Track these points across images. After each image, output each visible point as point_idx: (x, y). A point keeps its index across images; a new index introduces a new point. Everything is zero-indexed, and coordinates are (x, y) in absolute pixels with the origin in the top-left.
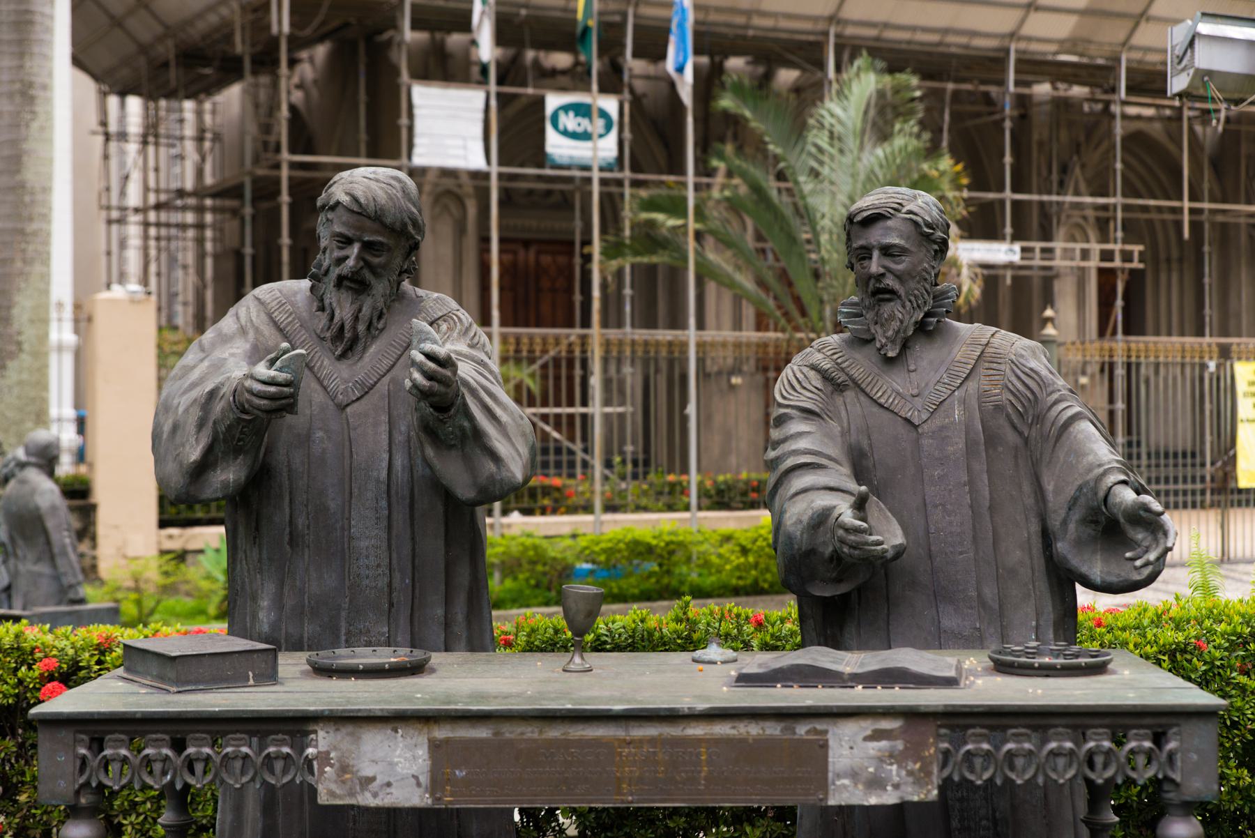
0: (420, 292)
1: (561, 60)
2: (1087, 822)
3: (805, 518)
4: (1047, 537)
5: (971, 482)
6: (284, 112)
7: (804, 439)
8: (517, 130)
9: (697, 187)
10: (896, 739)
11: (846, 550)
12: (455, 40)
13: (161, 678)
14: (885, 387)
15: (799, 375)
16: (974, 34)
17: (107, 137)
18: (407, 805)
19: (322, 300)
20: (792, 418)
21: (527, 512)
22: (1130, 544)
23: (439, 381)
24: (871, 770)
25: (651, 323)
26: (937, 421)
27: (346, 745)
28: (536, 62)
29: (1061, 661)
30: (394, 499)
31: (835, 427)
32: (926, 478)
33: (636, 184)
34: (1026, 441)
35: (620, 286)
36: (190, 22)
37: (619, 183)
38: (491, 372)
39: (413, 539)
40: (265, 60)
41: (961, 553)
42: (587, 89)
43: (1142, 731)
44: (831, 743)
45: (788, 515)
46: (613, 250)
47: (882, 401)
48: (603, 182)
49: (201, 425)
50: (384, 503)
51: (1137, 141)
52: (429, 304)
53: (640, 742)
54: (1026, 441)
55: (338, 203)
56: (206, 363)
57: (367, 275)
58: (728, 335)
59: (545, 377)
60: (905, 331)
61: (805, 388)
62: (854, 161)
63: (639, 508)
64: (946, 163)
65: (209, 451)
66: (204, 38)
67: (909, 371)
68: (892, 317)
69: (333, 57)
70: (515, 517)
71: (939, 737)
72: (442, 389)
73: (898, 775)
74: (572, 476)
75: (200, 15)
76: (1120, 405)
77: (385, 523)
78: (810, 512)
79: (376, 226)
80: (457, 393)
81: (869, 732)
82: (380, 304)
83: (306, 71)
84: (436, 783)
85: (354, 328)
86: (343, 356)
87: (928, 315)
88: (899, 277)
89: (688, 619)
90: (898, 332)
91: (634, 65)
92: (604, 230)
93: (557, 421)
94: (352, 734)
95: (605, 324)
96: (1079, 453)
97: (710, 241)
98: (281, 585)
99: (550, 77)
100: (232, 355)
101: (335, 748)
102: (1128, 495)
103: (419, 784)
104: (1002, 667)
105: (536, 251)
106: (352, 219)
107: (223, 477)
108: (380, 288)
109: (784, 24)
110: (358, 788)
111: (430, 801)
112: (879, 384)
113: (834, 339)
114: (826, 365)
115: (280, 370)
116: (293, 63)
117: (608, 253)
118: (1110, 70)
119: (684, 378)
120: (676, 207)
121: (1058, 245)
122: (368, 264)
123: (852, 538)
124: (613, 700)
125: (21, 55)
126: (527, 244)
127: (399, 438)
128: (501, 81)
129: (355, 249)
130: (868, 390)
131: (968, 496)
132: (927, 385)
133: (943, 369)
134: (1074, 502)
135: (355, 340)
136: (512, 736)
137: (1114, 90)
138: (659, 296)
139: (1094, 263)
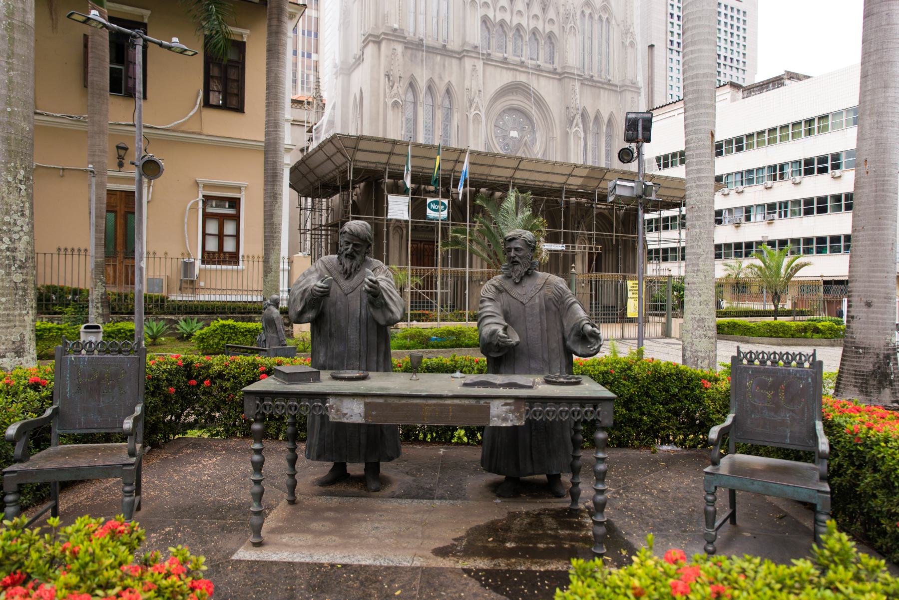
2: (574, 429)
6: (351, 202)
8: (418, 209)
13: (284, 379)
21: (418, 321)
22: (590, 343)
25: (457, 266)
26: (531, 303)
27: (338, 403)
29: (565, 381)
31: (499, 304)
33: (452, 225)
40: (346, 187)
49: (301, 300)
51: (600, 215)
58: (479, 270)
59: (424, 280)
62: (515, 222)
64: (541, 219)
65: (304, 308)
69: (365, 186)
70: (415, 322)
76: (594, 293)
80: (380, 291)
86: (347, 279)
88: (520, 257)
93: (427, 294)
96: (575, 314)
102: (589, 328)
104: (548, 382)
105: (422, 244)
108: (359, 258)
114: (497, 284)
116: (354, 188)
118: (593, 194)
120: (463, 232)
121: (577, 245)
124: (422, 391)
126: (421, 242)
127: (363, 305)
129: (351, 246)
134: (572, 329)
135: (351, 274)
138: (458, 258)
139: (587, 251)
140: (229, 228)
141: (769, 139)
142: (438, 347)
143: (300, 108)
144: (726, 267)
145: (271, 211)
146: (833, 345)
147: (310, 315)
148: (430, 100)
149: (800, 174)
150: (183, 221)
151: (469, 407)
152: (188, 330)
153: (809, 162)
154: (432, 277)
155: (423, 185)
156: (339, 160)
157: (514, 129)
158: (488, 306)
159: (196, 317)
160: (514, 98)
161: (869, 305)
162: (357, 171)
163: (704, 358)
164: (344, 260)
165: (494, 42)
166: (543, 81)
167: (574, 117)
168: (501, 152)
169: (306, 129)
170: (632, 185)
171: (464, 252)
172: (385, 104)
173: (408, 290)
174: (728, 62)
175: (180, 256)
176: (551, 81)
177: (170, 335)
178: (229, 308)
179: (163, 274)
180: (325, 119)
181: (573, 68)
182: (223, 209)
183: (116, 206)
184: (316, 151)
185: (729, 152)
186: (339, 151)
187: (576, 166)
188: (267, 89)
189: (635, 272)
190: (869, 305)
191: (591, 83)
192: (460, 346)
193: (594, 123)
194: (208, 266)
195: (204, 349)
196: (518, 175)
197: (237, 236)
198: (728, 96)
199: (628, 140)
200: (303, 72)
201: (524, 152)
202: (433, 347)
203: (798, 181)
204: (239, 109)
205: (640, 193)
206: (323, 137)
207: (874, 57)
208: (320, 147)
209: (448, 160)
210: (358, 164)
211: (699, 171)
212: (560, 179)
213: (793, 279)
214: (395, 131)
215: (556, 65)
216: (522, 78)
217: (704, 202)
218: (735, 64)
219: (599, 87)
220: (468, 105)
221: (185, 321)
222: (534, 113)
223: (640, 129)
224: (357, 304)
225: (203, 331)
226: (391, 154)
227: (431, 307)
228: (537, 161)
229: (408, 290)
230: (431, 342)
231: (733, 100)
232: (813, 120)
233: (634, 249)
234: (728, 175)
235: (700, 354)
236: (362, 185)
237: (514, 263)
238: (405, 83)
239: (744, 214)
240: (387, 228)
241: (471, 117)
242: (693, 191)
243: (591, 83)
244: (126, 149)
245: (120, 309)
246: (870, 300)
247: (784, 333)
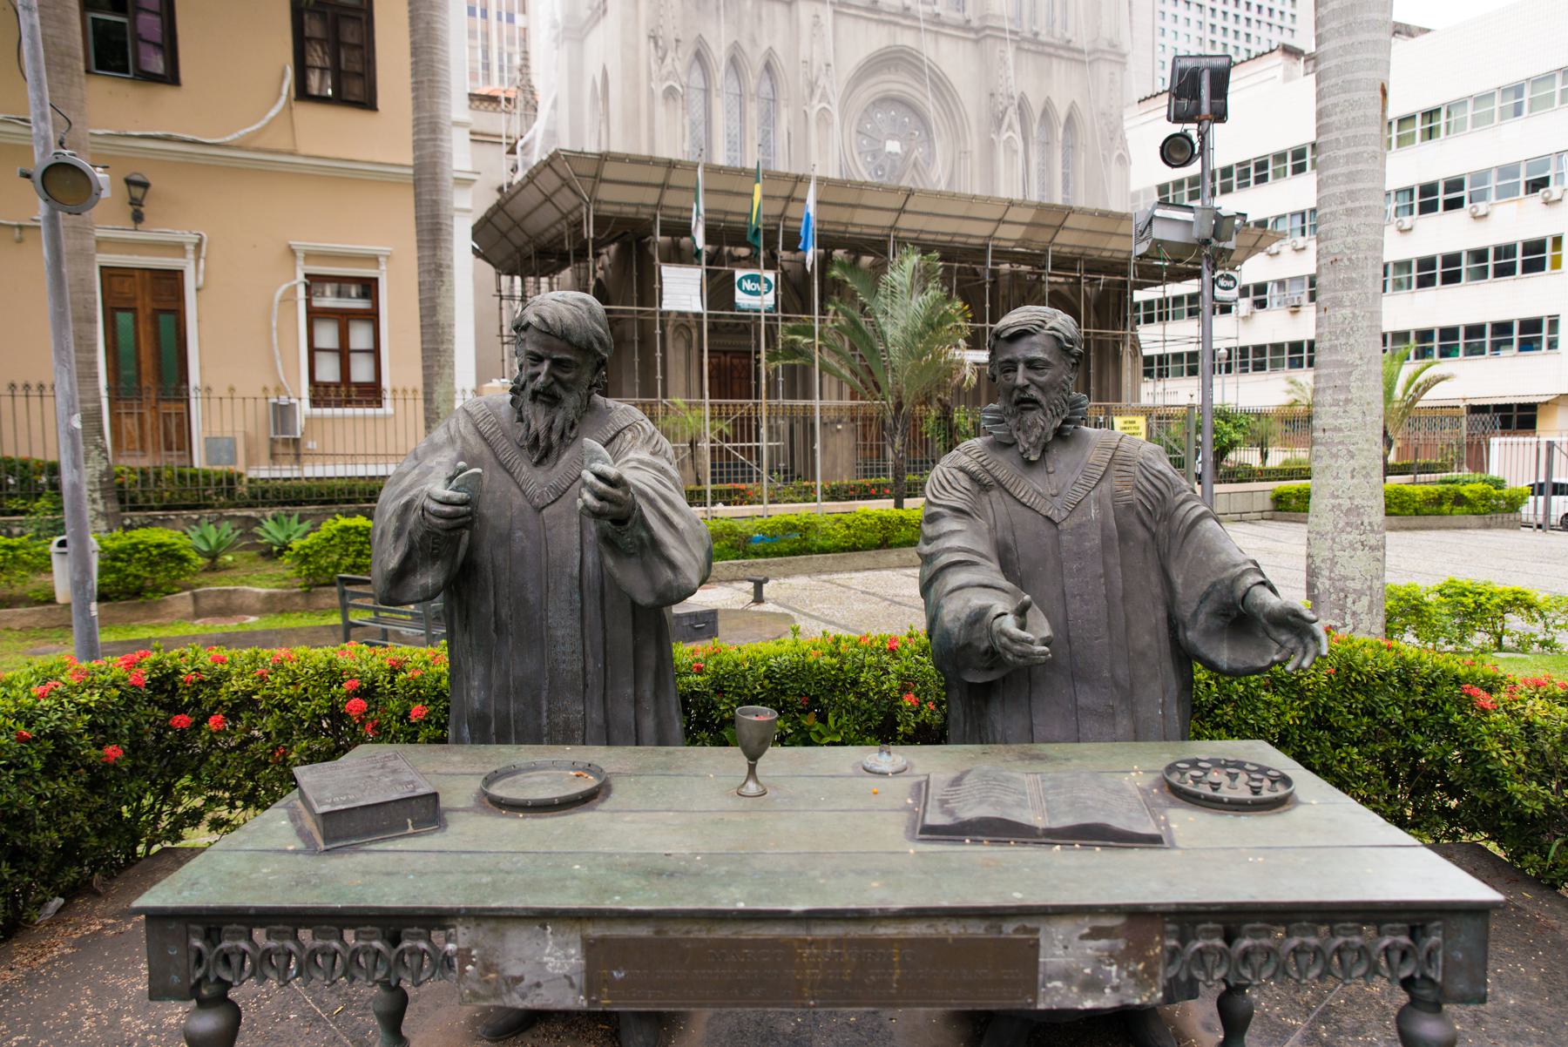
0: (611, 402)
1: (743, 252)
3: (963, 616)
4: (1174, 625)
5: (1106, 575)
8: (719, 290)
9: (820, 321)
10: (1117, 937)
11: (1009, 657)
12: (685, 241)
16: (970, 236)
17: (501, 298)
18: (560, 1007)
19: (520, 412)
21: (726, 504)
23: (610, 502)
24: (1088, 971)
25: (793, 396)
26: (1075, 520)
28: (730, 253)
30: (586, 593)
33: (785, 319)
34: (1154, 536)
35: (776, 376)
36: (541, 234)
37: (776, 319)
38: (671, 478)
39: (604, 628)
40: (581, 255)
42: (758, 267)
43: (1398, 926)
44: (1042, 942)
46: (772, 357)
48: (767, 318)
49: (398, 536)
50: (577, 597)
52: (616, 414)
53: (821, 943)
54: (1154, 536)
55: (529, 324)
56: (417, 471)
57: (558, 389)
58: (835, 402)
59: (735, 426)
64: (959, 304)
65: (407, 559)
66: (550, 241)
68: (1035, 424)
69: (619, 251)
70: (720, 506)
71: (1164, 934)
72: (614, 509)
73: (1118, 976)
74: (750, 481)
75: (546, 230)
77: (578, 614)
78: (967, 611)
79: (563, 344)
80: (634, 506)
81: (1086, 931)
82: (572, 416)
83: (605, 259)
84: (593, 981)
85: (548, 437)
86: (539, 463)
87: (1065, 422)
88: (1041, 388)
91: (783, 254)
92: (767, 346)
93: (735, 448)
94: (494, 930)
95: (768, 397)
97: (825, 350)
98: (489, 666)
99: (738, 261)
100: (440, 464)
101: (476, 945)
103: (572, 985)
106: (542, 338)
107: (423, 582)
108: (571, 401)
109: (866, 230)
110: (504, 989)
111: (585, 1004)
113: (977, 442)
114: (973, 467)
115: (456, 489)
116: (597, 255)
118: (1043, 256)
119: (813, 425)
120: (808, 332)
122: (557, 380)
125: (435, 248)
126: (725, 353)
128: (709, 263)
129: (546, 366)
134: (1206, 596)
135: (549, 449)
136: (678, 935)
137: (1044, 267)
138: (798, 382)
140: (360, 336)
141: (1399, 137)
142: (767, 555)
143: (495, 110)
144: (1290, 387)
145: (432, 299)
146: (1487, 527)
147: (428, 578)
148: (736, 84)
149: (1411, 213)
150: (269, 324)
151: (961, 943)
152: (281, 537)
153: (1428, 190)
154: (749, 419)
155: (731, 243)
156: (566, 200)
157: (892, 137)
158: (953, 532)
159: (299, 510)
160: (893, 77)
162: (601, 222)
163: (1360, 594)
164: (528, 410)
166: (946, 45)
167: (1004, 113)
168: (869, 179)
169: (505, 149)
170: (1188, 216)
172: (651, 92)
173: (705, 445)
174: (1265, 17)
175: (260, 394)
176: (961, 43)
177: (246, 548)
178: (362, 492)
179: (239, 428)
180: (539, 126)
181: (1001, 18)
182: (343, 301)
183: (135, 299)
184: (523, 186)
185: (1278, 175)
186: (566, 183)
187: (1011, 203)
188: (413, 54)
189: (1119, 399)
191: (1036, 47)
192: (808, 551)
193: (1041, 125)
194: (328, 411)
195: (309, 575)
196: (906, 222)
197: (375, 352)
198: (1279, 72)
199: (1178, 119)
200: (500, 48)
201: (913, 179)
202: (757, 555)
203: (1406, 226)
204: (367, 102)
205: (1207, 232)
206: (537, 156)
208: (531, 178)
209: (773, 197)
210: (603, 207)
211: (1351, 177)
212: (983, 230)
213: (1419, 404)
214: (670, 140)
215: (969, 13)
216: (906, 39)
217: (1363, 246)
218: (1276, 19)
219: (1050, 55)
220: (807, 92)
221: (275, 519)
222: (931, 106)
223: (1205, 92)
224: (569, 539)
225: (306, 542)
226: (664, 186)
229: (705, 445)
230: (753, 546)
231: (1288, 78)
232: (1438, 110)
233: (1117, 358)
234: (1278, 218)
235: (1350, 584)
236: (613, 248)
237: (1025, 403)
238: (687, 51)
239: (1307, 289)
240: (663, 328)
241: (813, 115)
242: (1338, 224)
243: (1036, 47)
244: (145, 185)
245: (148, 500)
247: (1402, 508)
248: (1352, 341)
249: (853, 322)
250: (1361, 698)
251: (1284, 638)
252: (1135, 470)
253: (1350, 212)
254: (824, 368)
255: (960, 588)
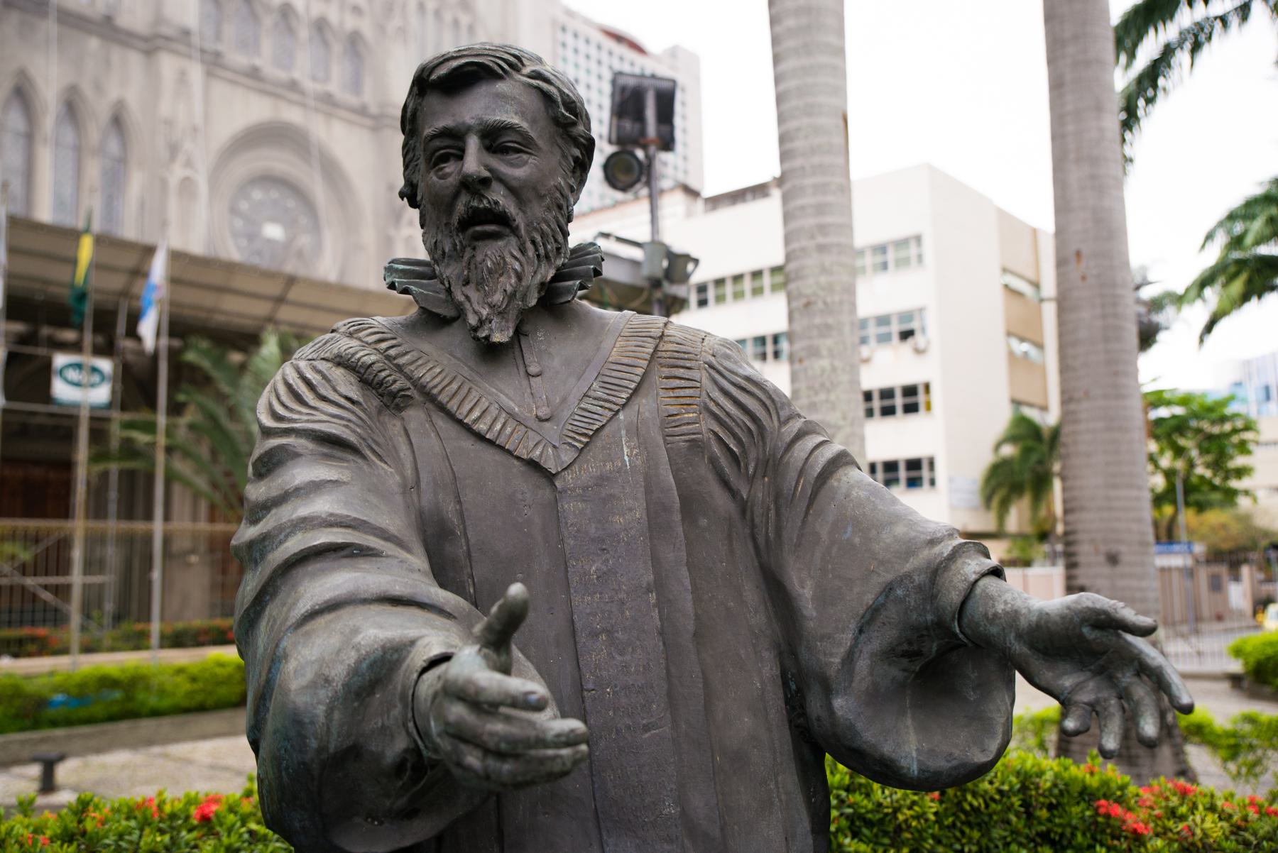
3: (339, 672)
4: (799, 686)
7: (319, 495)
11: (473, 759)
14: (484, 403)
15: (310, 375)
20: (296, 455)
21: (16, 655)
26: (591, 468)
31: (389, 475)
32: (574, 580)
34: (744, 508)
41: (647, 728)
45: (291, 665)
46: (98, 456)
47: (481, 427)
54: (744, 508)
60: (524, 297)
61: (324, 399)
63: (112, 649)
67: (528, 375)
78: (351, 657)
87: (559, 277)
88: (514, 191)
89: (84, 833)
90: (512, 296)
93: (46, 587)
112: (474, 396)
117: (95, 458)
123: (498, 727)
130: (453, 406)
131: (655, 614)
132: (564, 400)
133: (591, 374)
134: (871, 617)
138: (135, 495)
157: (274, 220)
158: (316, 487)
161: (1113, 559)
165: (230, 30)
171: (150, 478)
190: (1113, 559)
202: (54, 724)
207: (1071, 50)
211: (820, 209)
216: (292, 115)
222: (319, 191)
227: (58, 618)
228: (325, 286)
230: (50, 712)
231: (689, 214)
246: (1114, 548)
248: (833, 397)
249: (212, 418)
250: (976, 834)
251: (1068, 682)
252: (703, 377)
253: (822, 248)
254: (170, 479)
255: (333, 606)
